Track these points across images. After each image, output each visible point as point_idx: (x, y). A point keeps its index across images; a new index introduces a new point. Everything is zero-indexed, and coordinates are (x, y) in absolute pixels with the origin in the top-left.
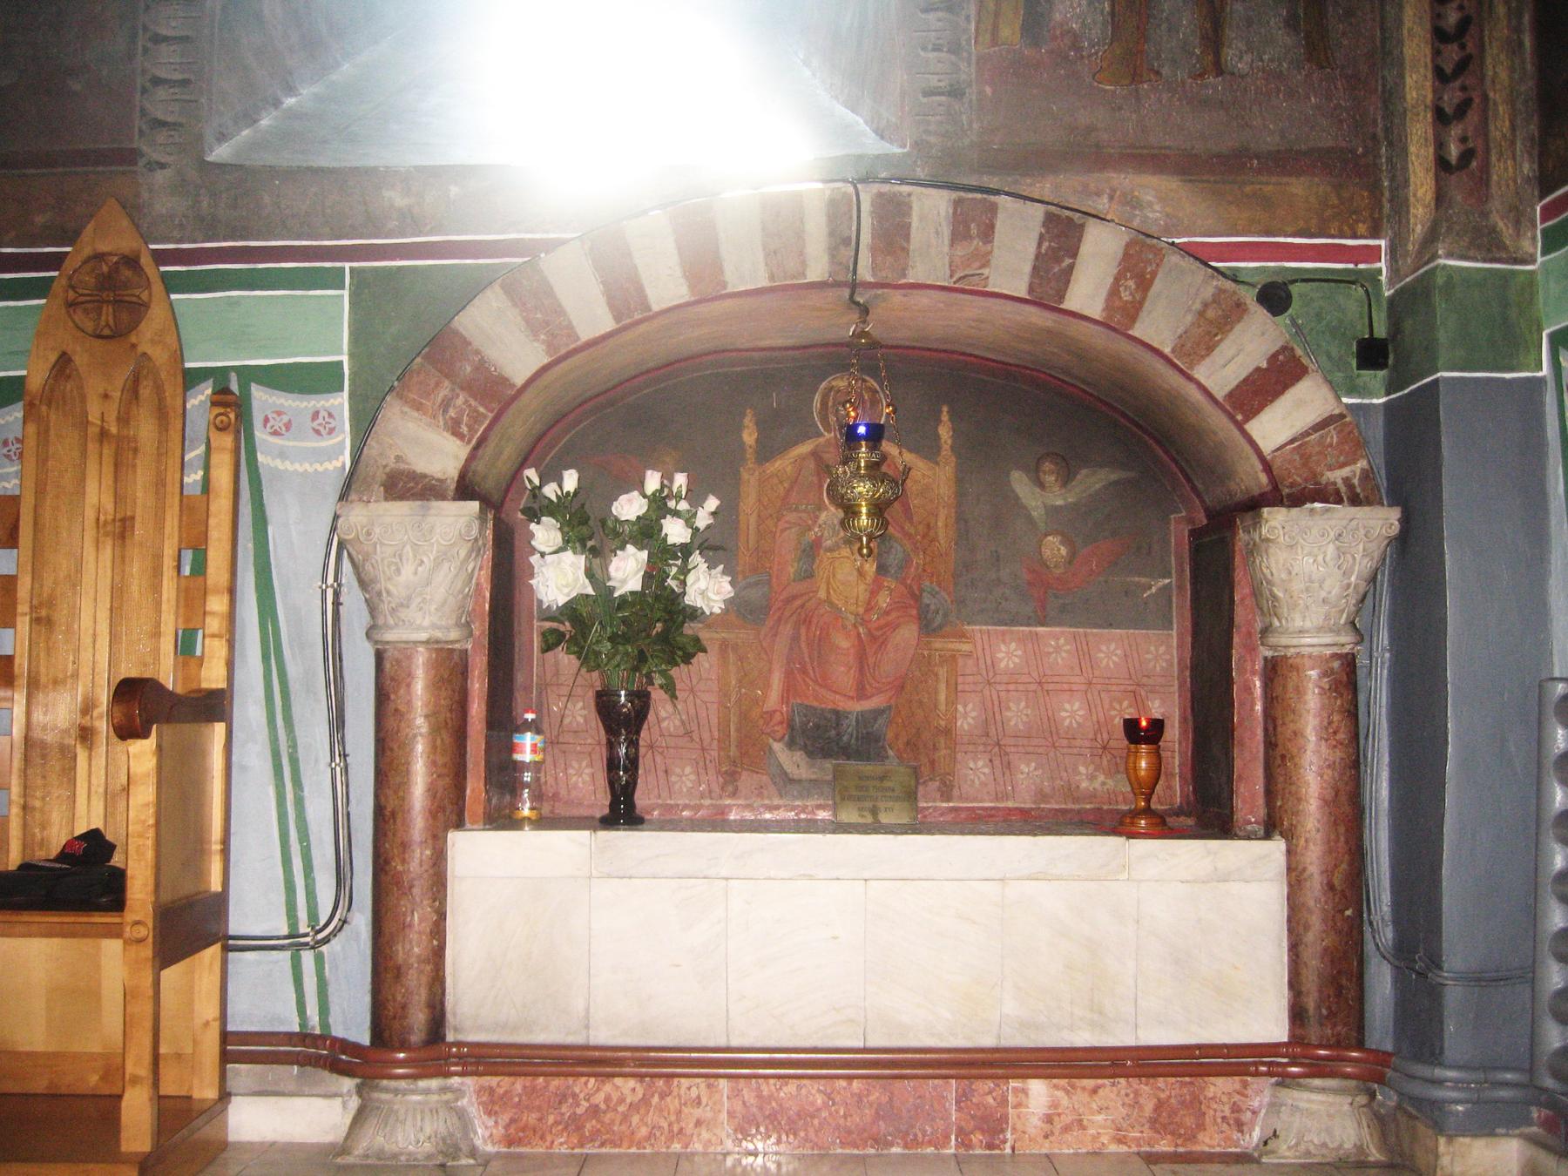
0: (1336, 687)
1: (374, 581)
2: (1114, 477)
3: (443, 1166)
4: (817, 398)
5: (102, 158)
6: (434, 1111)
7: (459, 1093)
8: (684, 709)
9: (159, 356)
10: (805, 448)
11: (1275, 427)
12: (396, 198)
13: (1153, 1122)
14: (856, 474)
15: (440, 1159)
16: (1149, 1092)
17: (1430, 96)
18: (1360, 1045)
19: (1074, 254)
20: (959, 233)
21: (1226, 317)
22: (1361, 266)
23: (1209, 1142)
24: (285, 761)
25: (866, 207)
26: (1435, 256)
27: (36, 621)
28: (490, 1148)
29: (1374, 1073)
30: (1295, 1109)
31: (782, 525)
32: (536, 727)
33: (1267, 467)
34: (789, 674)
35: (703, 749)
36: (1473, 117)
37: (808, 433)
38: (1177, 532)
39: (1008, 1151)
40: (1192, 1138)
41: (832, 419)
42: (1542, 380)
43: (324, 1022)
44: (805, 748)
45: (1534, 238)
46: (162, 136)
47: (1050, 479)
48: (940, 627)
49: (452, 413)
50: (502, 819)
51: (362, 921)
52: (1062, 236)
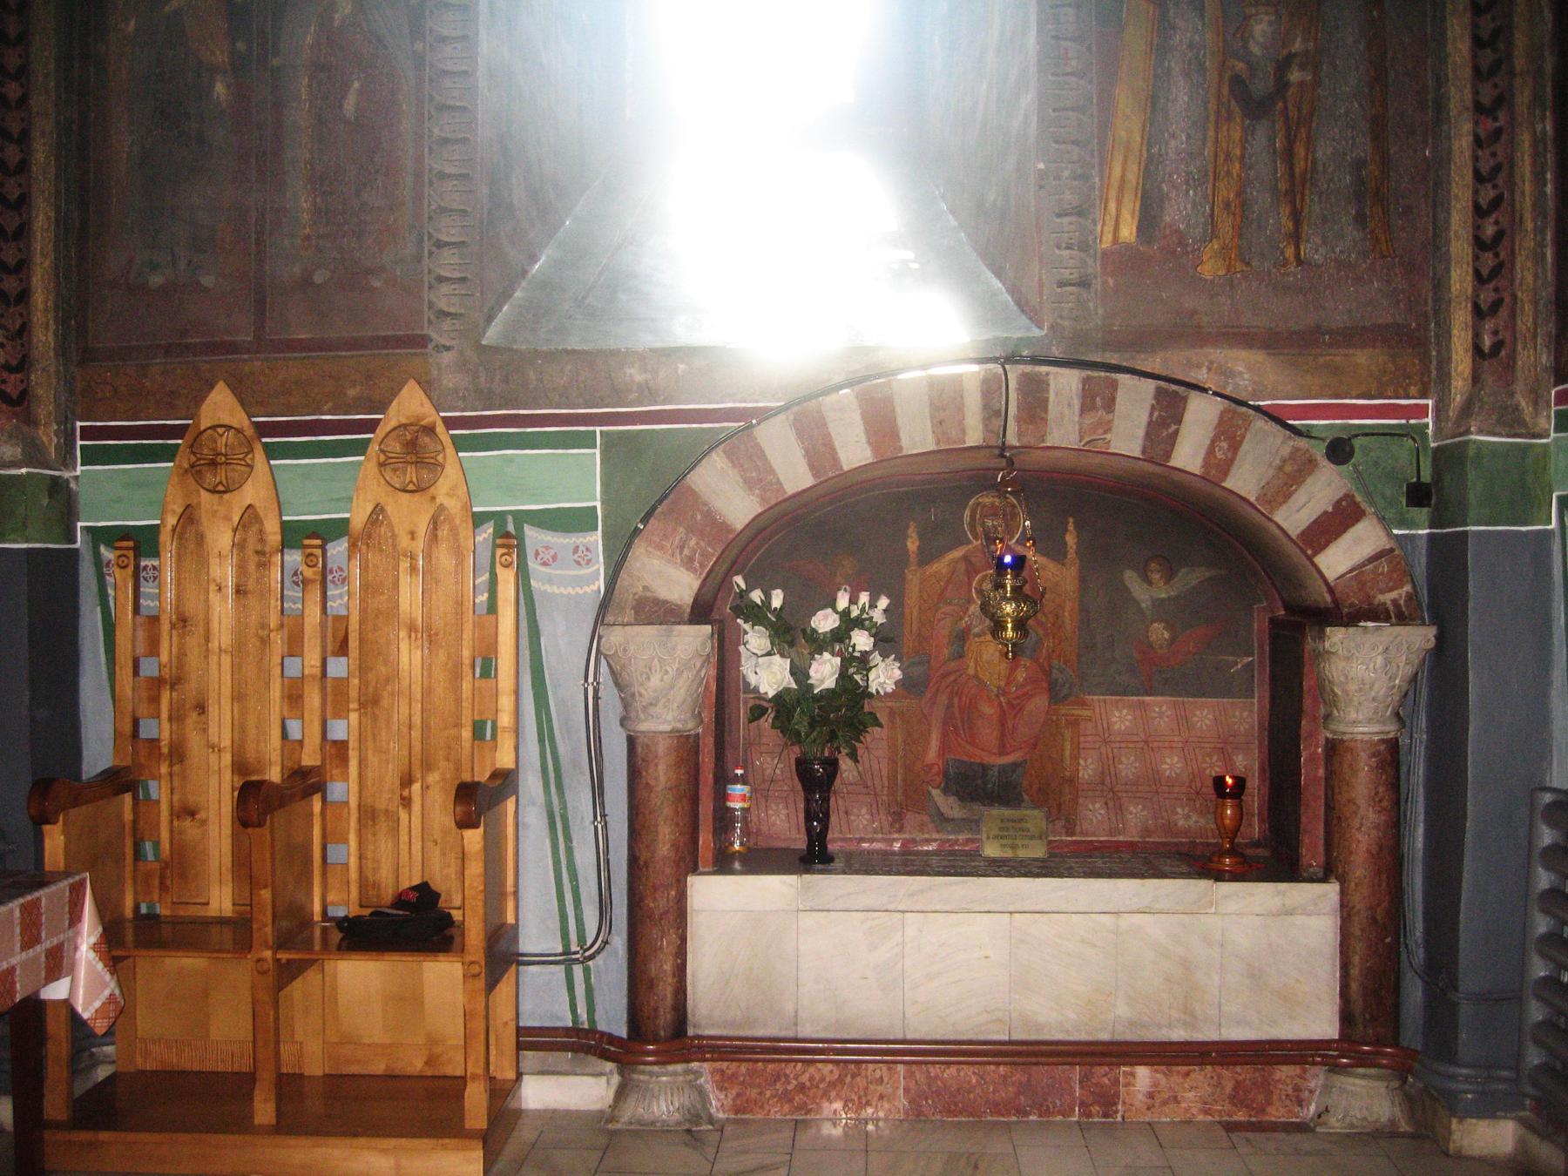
0: (1381, 765)
1: (630, 685)
2: (1208, 574)
3: (689, 1131)
4: (967, 513)
5: (400, 342)
6: (680, 1089)
7: (698, 1074)
8: (864, 767)
9: (453, 505)
10: (957, 553)
11: (1336, 561)
12: (635, 374)
13: (1233, 1098)
14: (1004, 598)
15: (687, 1126)
16: (1229, 1076)
17: (1470, 290)
18: (1395, 1043)
19: (1179, 421)
20: (1087, 406)
21: (1300, 471)
22: (1412, 422)
23: (1276, 1113)
24: (558, 819)
25: (1013, 384)
26: (1468, 432)
27: (362, 706)
28: (721, 1115)
29: (1401, 1070)
30: (1342, 1090)
31: (939, 616)
32: (743, 780)
33: (1331, 590)
34: (945, 734)
35: (876, 794)
36: (1504, 313)
37: (961, 541)
38: (1259, 625)
39: (1119, 1119)
40: (1262, 1111)
41: (979, 529)
42: (1552, 531)
43: (591, 1019)
44: (956, 794)
45: (1549, 417)
46: (447, 324)
47: (1156, 577)
48: (1066, 697)
49: (686, 552)
50: (723, 864)
51: (619, 942)
52: (1171, 402)
